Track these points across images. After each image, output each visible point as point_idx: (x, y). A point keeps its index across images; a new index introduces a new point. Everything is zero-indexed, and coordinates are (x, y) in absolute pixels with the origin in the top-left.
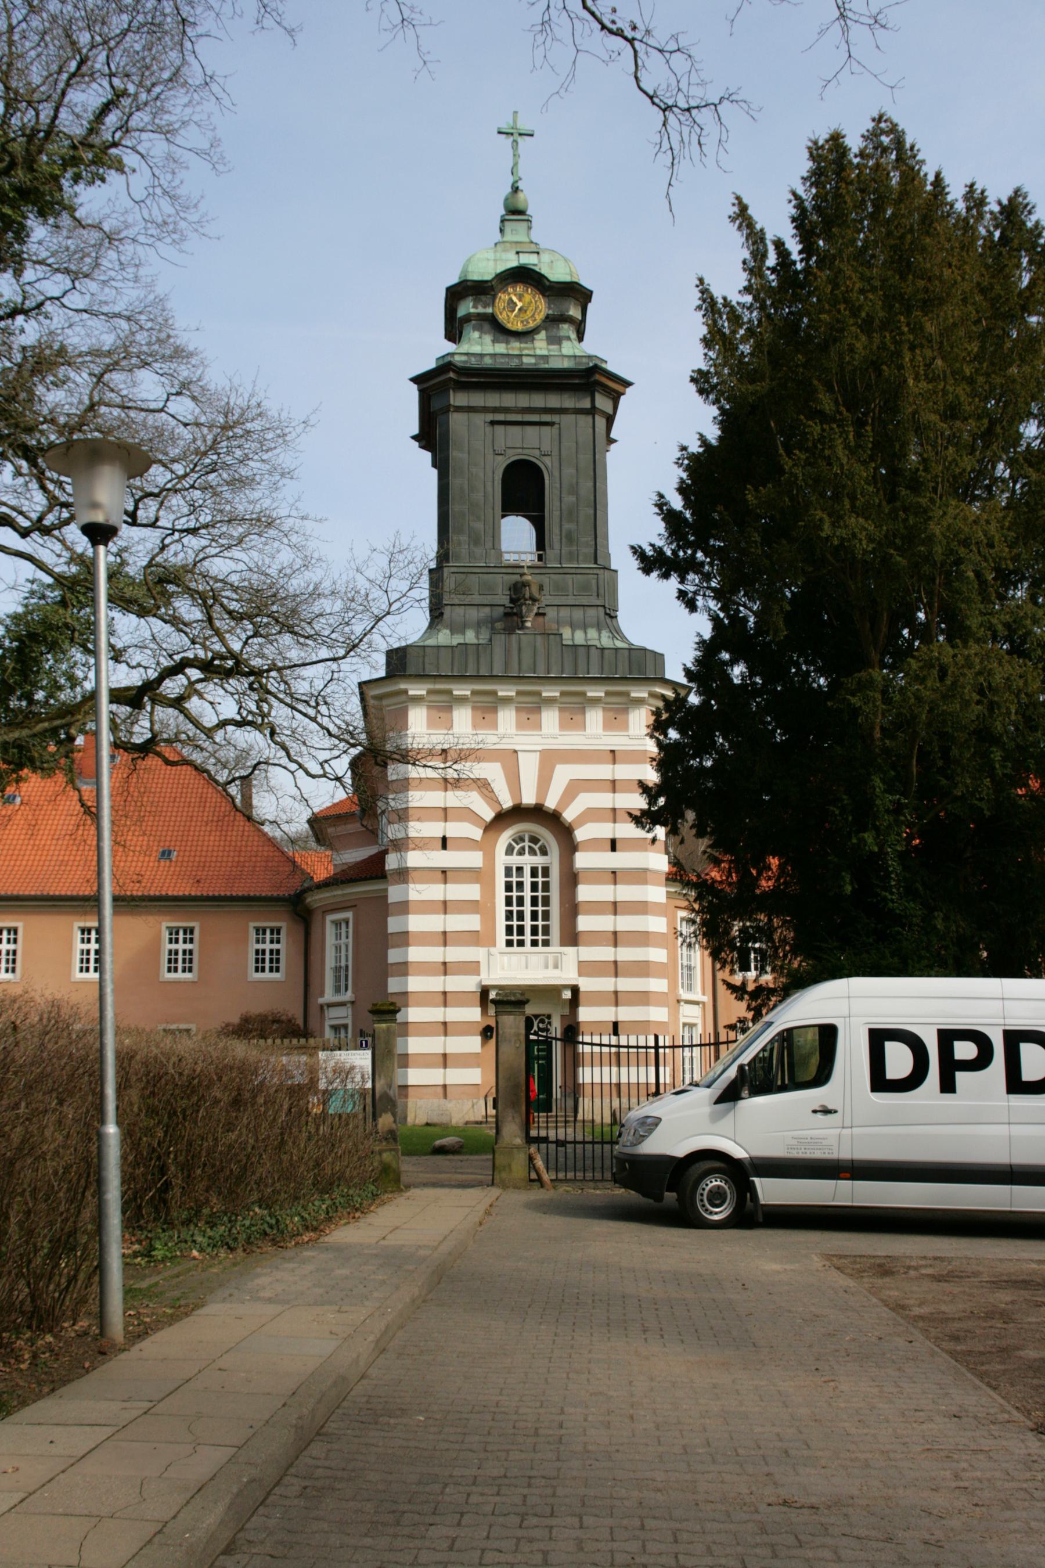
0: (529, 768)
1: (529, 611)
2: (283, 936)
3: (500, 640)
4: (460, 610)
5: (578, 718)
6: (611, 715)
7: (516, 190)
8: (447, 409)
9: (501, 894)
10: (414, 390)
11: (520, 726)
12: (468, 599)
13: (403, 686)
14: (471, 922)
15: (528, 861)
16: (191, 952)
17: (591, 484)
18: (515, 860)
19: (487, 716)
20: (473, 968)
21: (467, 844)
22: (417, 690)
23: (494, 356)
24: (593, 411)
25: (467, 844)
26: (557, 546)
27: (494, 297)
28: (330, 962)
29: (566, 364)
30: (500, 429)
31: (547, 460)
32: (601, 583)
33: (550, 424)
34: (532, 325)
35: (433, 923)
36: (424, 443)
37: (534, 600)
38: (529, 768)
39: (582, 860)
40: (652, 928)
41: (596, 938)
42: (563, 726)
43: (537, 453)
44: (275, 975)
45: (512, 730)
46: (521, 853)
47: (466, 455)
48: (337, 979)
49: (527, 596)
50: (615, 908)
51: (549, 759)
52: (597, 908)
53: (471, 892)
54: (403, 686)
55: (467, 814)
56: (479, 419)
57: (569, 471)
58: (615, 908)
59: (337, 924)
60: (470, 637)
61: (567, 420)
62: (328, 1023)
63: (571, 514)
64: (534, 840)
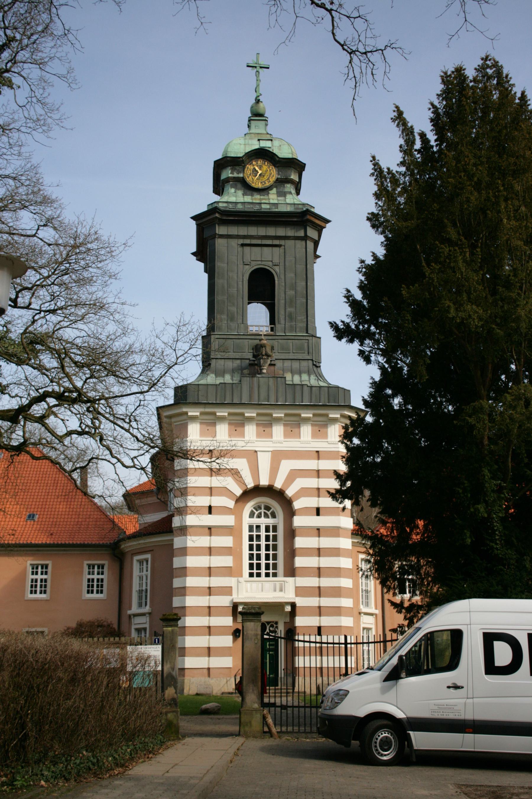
0: (264, 463)
1: (265, 362)
2: (106, 570)
3: (246, 381)
4: (222, 362)
5: (296, 430)
6: (317, 428)
7: (258, 101)
8: (214, 236)
9: (246, 543)
10: (193, 224)
11: (259, 435)
12: (226, 355)
13: (185, 410)
14: (227, 561)
15: (263, 521)
16: (46, 580)
17: (304, 283)
18: (255, 521)
19: (238, 429)
20: (227, 591)
21: (225, 510)
22: (193, 412)
23: (243, 203)
24: (305, 238)
25: (225, 510)
26: (282, 322)
27: (244, 167)
28: (135, 587)
29: (289, 209)
30: (247, 249)
31: (277, 268)
32: (310, 346)
33: (279, 246)
34: (267, 184)
35: (203, 561)
36: (199, 257)
37: (268, 356)
38: (264, 463)
39: (298, 521)
40: (342, 546)
41: (307, 572)
42: (286, 436)
43: (270, 263)
44: (100, 596)
45: (310, 438)
46: (259, 516)
47: (226, 265)
48: (140, 598)
49: (264, 353)
50: (319, 552)
51: (278, 457)
52: (307, 552)
53: (227, 541)
54: (185, 410)
55: (225, 491)
56: (234, 243)
57: (290, 275)
58: (319, 552)
59: (141, 562)
60: (228, 379)
61: (290, 243)
62: (133, 627)
63: (292, 302)
64: (267, 508)
